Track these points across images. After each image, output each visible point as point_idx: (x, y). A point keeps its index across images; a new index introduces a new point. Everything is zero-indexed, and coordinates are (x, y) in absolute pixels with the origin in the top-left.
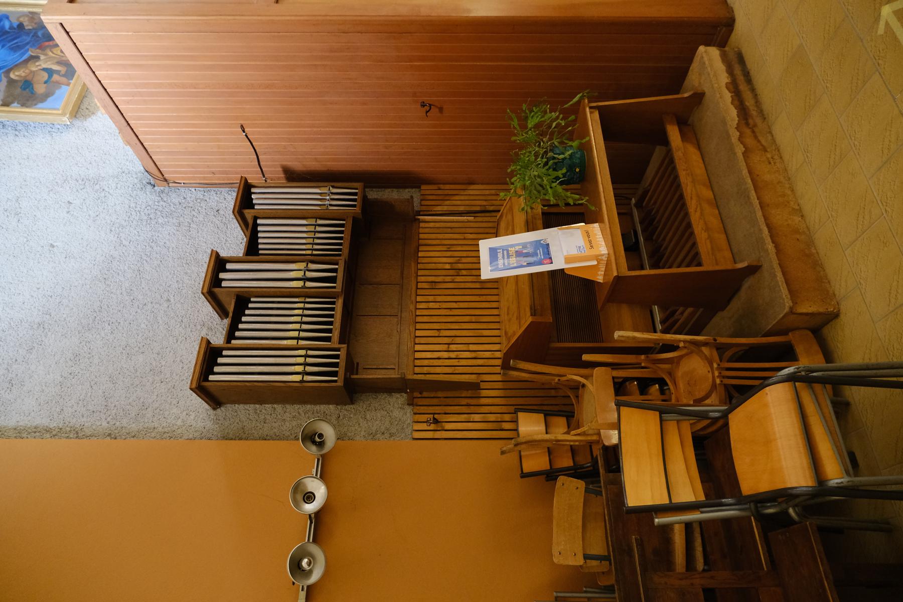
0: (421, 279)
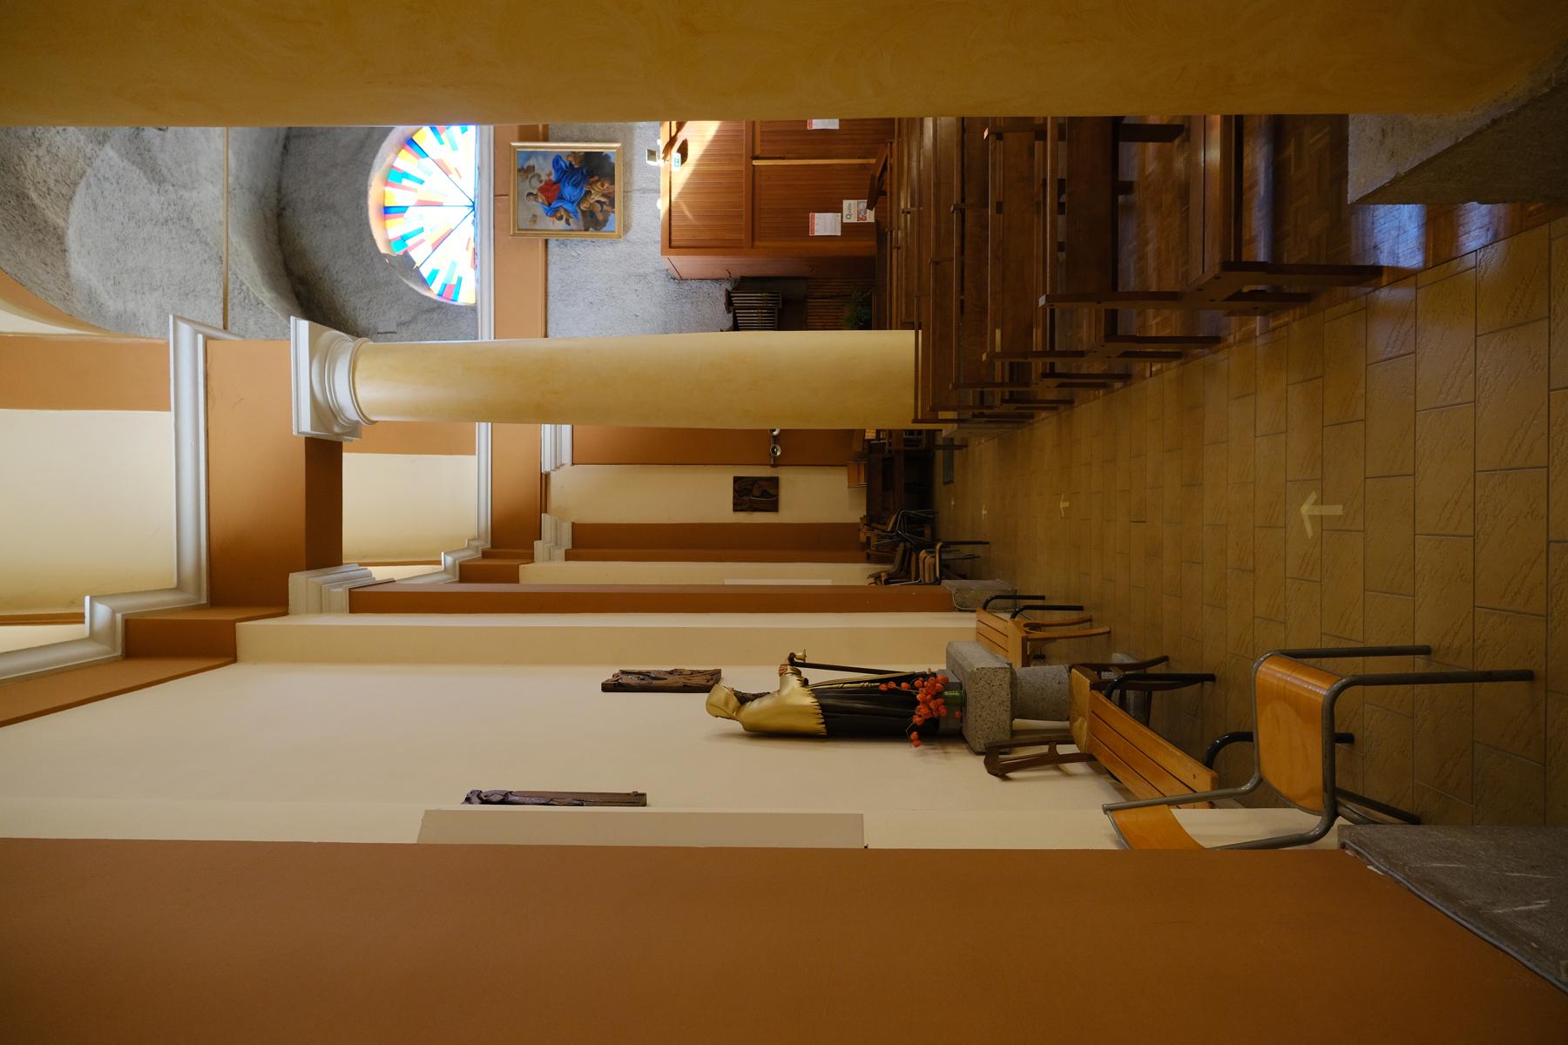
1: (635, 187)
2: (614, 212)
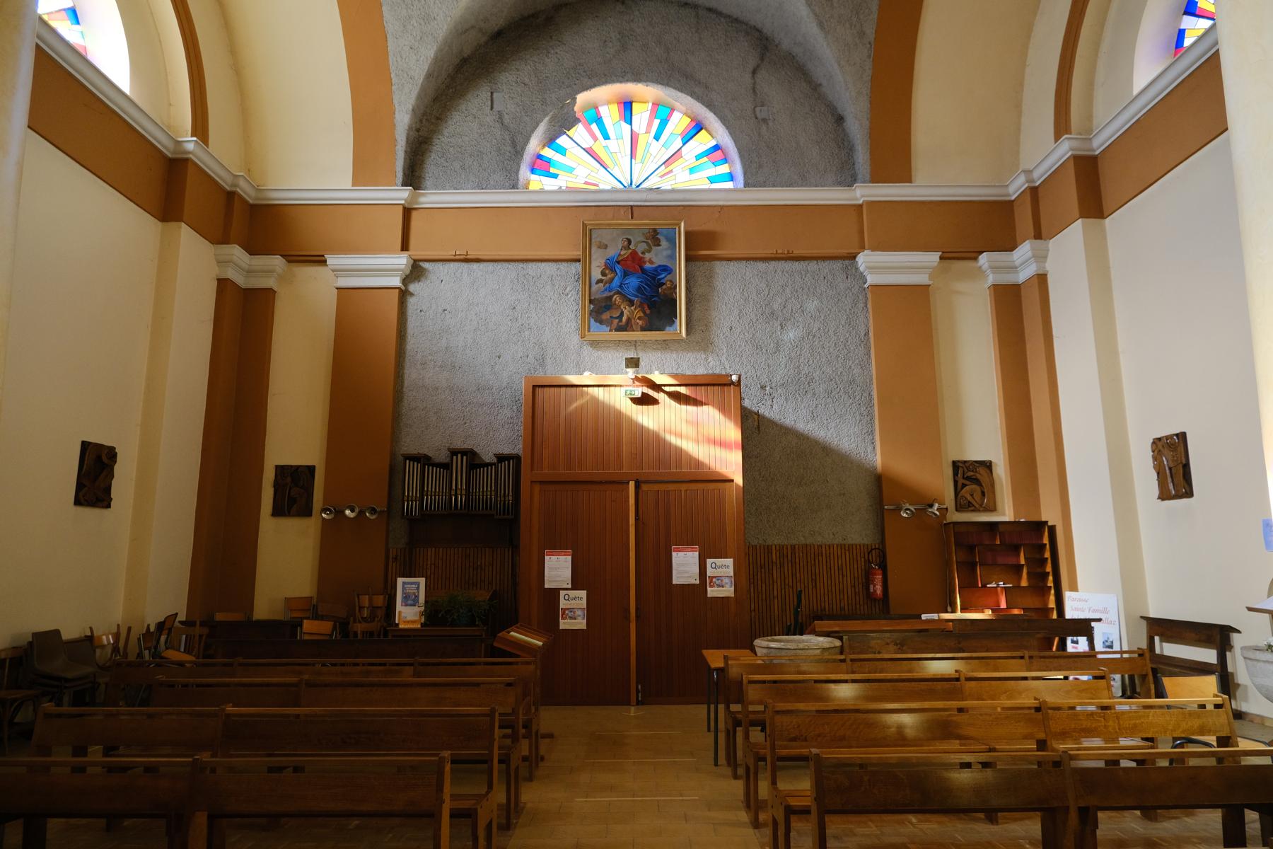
0: (472, 549)
2: (611, 330)
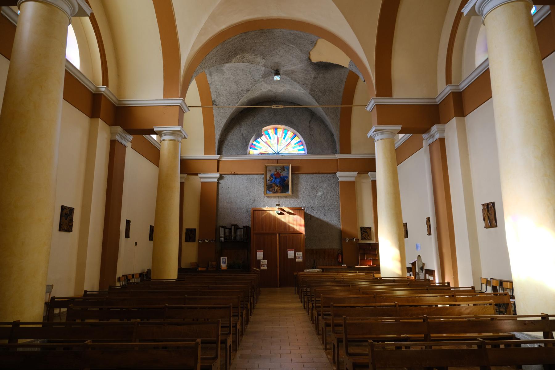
1: (280, 199)
2: (272, 193)
